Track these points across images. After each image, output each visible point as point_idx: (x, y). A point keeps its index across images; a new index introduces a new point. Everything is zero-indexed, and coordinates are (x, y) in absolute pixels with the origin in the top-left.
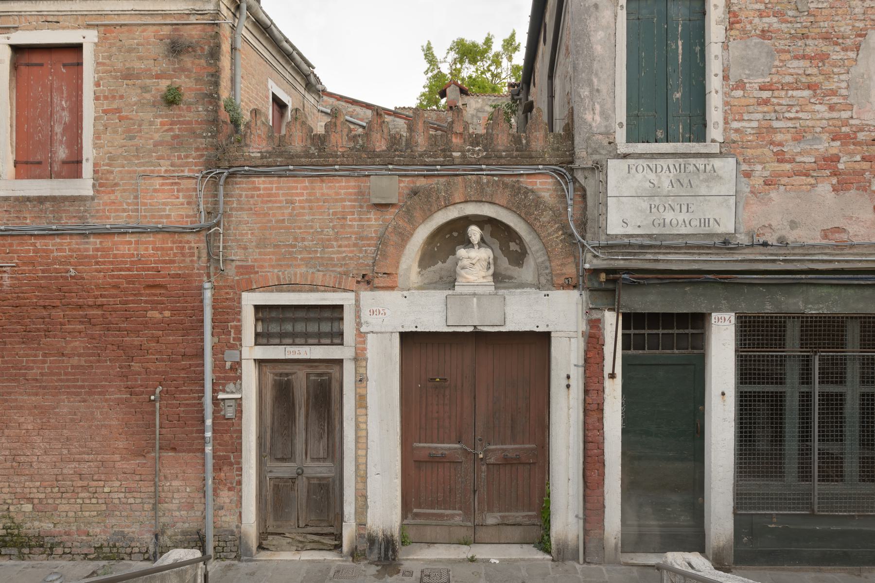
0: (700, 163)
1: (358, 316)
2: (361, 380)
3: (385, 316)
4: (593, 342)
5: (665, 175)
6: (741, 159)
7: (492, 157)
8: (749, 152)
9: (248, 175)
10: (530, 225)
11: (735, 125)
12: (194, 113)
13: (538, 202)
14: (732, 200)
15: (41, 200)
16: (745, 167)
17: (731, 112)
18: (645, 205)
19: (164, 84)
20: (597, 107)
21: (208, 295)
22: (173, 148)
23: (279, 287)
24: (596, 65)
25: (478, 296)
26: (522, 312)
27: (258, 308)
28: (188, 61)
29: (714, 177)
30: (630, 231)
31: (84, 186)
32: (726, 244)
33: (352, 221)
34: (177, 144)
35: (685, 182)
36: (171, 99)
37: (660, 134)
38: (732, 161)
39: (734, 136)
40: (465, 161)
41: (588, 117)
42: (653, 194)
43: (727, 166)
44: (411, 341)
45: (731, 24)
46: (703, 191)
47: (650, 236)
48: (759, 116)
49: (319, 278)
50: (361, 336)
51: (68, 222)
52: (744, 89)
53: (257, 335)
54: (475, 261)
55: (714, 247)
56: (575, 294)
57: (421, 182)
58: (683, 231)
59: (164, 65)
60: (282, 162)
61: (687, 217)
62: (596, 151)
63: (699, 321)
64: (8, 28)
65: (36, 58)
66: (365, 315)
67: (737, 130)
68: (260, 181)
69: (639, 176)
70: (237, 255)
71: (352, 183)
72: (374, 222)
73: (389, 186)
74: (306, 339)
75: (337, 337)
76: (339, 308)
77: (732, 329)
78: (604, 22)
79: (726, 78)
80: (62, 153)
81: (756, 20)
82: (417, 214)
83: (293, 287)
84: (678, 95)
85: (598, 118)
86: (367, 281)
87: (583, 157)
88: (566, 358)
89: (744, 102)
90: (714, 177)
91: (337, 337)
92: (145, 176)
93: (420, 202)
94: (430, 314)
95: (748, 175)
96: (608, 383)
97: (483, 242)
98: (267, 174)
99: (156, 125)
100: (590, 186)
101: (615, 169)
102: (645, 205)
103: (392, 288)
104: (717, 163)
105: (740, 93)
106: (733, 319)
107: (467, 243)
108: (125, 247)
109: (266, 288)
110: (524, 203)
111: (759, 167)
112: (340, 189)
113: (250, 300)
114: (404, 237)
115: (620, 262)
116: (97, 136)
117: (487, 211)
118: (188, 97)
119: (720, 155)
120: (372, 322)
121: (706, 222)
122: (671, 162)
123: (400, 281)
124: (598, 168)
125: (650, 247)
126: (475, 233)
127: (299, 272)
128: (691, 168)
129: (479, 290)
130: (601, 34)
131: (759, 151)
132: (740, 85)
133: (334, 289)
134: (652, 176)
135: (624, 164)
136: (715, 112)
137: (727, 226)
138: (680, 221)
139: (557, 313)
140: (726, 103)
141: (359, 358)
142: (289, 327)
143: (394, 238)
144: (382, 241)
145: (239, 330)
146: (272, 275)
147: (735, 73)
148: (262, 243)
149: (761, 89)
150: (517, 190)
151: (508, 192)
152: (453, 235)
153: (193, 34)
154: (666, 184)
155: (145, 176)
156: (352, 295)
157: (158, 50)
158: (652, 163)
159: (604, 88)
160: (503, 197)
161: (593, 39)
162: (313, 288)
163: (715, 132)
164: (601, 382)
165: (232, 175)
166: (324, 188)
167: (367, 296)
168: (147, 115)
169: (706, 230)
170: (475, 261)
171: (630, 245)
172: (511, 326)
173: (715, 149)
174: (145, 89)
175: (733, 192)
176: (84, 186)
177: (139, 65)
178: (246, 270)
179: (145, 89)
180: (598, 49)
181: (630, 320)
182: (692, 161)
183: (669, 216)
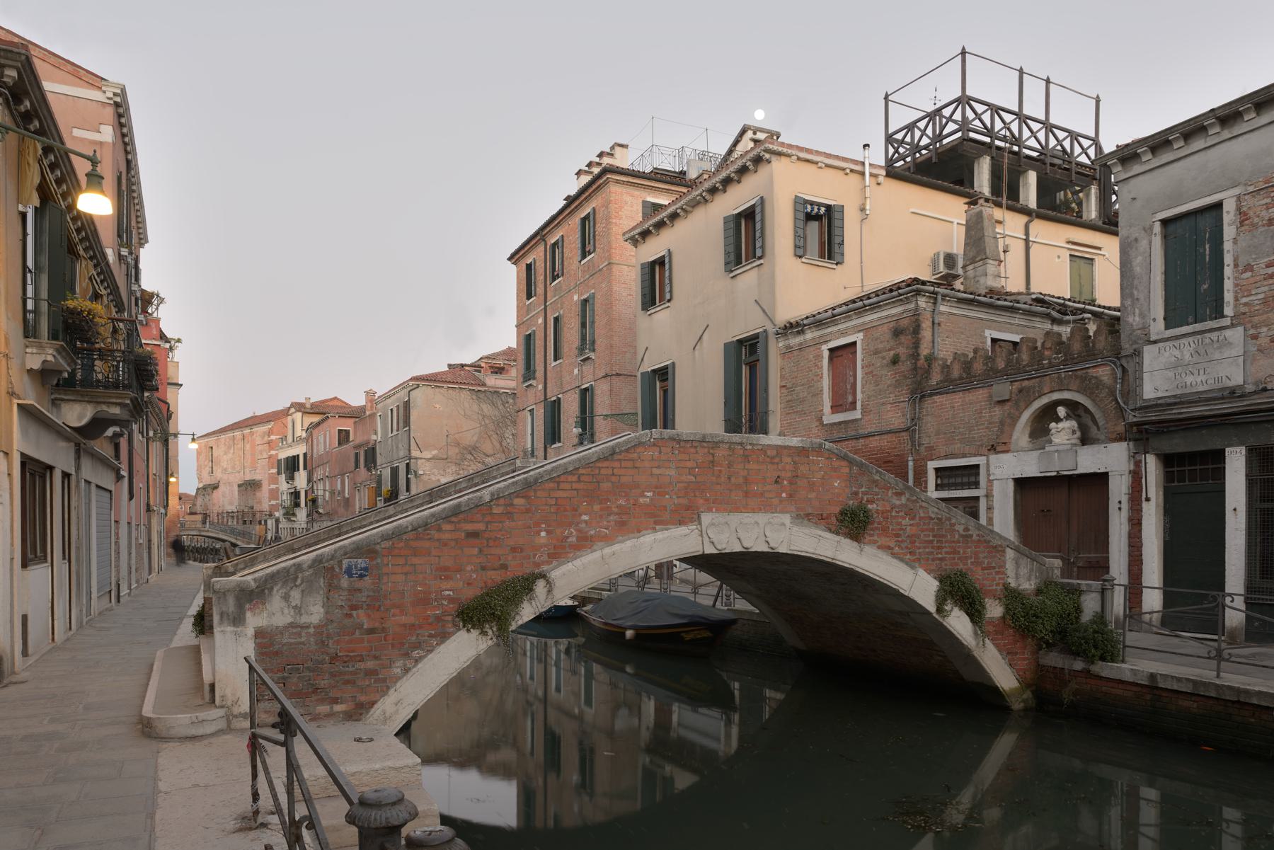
0: (1214, 336)
1: (988, 470)
2: (990, 508)
3: (1005, 469)
4: (1137, 477)
5: (1186, 350)
6: (1249, 326)
7: (1069, 360)
8: (1256, 319)
9: (931, 395)
10: (1093, 400)
11: (1244, 300)
12: (905, 366)
13: (1099, 383)
14: (1241, 359)
15: (840, 423)
16: (1252, 331)
17: (1240, 289)
18: (1171, 374)
19: (892, 353)
20: (1137, 311)
21: (911, 463)
22: (896, 387)
23: (946, 457)
24: (1136, 282)
25: (1065, 452)
26: (1089, 461)
27: (937, 470)
28: (902, 338)
29: (1227, 344)
30: (1160, 394)
31: (857, 414)
32: (1233, 393)
33: (986, 414)
34: (898, 384)
35: (1202, 352)
36: (895, 361)
37: (1190, 319)
38: (1240, 329)
39: (1243, 309)
40: (1051, 365)
41: (1130, 319)
42: (1177, 365)
43: (1236, 335)
44: (1022, 484)
45: (1242, 223)
46: (1217, 356)
47: (1175, 396)
48: (1266, 288)
49: (967, 450)
50: (990, 482)
51: (851, 433)
52: (1252, 271)
53: (937, 485)
54: (1063, 431)
55: (1223, 398)
56: (1124, 444)
57: (1026, 383)
58: (1201, 389)
59: (892, 343)
60: (950, 385)
61: (1202, 378)
62: (1135, 342)
63: (1218, 457)
64: (860, 311)
65: (839, 353)
66: (992, 470)
67: (1245, 304)
68: (936, 398)
69: (1167, 354)
70: (925, 441)
71: (986, 390)
72: (998, 412)
73: (1003, 389)
74: (962, 486)
75: (976, 485)
76: (978, 466)
77: (1243, 459)
78: (1141, 249)
79: (1236, 266)
80: (850, 399)
81: (1264, 213)
82: (1022, 404)
83: (953, 456)
84: (1206, 286)
85: (1137, 319)
86: (993, 449)
87: (1127, 348)
88: (1119, 489)
89: (1252, 280)
90: (1227, 344)
91: (976, 485)
92: (883, 404)
93: (1026, 396)
94: (1031, 466)
95: (1255, 337)
96: (1144, 504)
97: (1068, 417)
98: (940, 393)
99: (888, 376)
100: (1130, 367)
101: (1149, 353)
102: (1171, 374)
103: (1007, 451)
104: (1228, 333)
105: (1249, 274)
106: (1244, 452)
107: (1058, 420)
108: (874, 443)
109: (940, 458)
110: (1089, 386)
111: (1265, 329)
112: (980, 395)
113: (932, 465)
114: (1014, 420)
115: (1152, 416)
116: (863, 387)
117: (1066, 395)
118: (903, 358)
119: (1233, 326)
120: (997, 473)
121: (1220, 379)
122: (1190, 339)
123: (1012, 447)
124: (1138, 353)
125: (1175, 404)
126: (1061, 411)
127: (957, 447)
128: (1207, 341)
129: (1060, 448)
130: (1140, 258)
131: (1265, 317)
132: (1249, 268)
133: (975, 455)
134: (1177, 353)
135: (1154, 348)
136: (1228, 296)
137: (1237, 379)
138: (1198, 382)
139: (1110, 458)
140: (1236, 285)
141: (989, 496)
142: (959, 480)
143: (1008, 421)
144: (1002, 423)
145: (926, 482)
146: (943, 450)
147: (1242, 261)
148: (938, 433)
149: (1267, 267)
150: (1084, 379)
151: (1078, 381)
152: (1047, 414)
153: (905, 323)
154: (1187, 357)
155: (883, 404)
156: (984, 458)
157: (888, 336)
158: (1176, 343)
159: (1141, 297)
160: (1075, 384)
161: (1134, 264)
162: (964, 456)
163: (1228, 311)
164: (1140, 505)
165: (923, 396)
166: (970, 397)
167: (993, 458)
168: (884, 372)
169: (1220, 385)
170: (1063, 431)
171: (1161, 405)
172: (1080, 471)
173: (1226, 322)
174: (883, 358)
175: (1241, 353)
176: (857, 414)
177: (880, 346)
178: (930, 449)
179: (883, 358)
180: (1138, 269)
181: (1168, 460)
182: (1208, 335)
183: (1189, 379)
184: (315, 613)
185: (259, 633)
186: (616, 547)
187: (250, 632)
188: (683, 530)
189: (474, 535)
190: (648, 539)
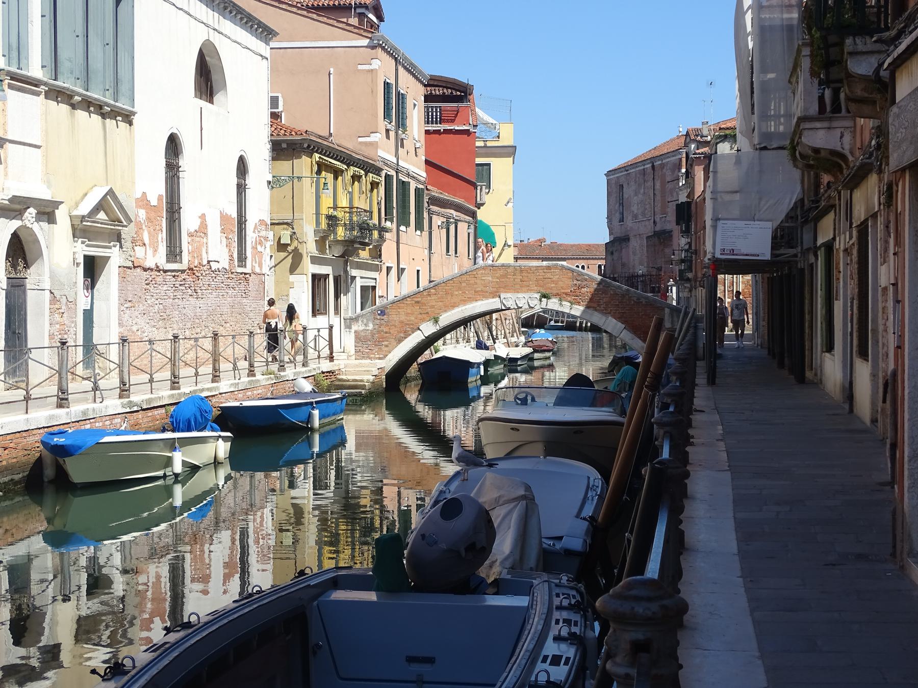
184: (371, 326)
185: (355, 332)
186: (467, 307)
187: (353, 331)
188: (494, 300)
189: (418, 302)
190: (480, 303)
